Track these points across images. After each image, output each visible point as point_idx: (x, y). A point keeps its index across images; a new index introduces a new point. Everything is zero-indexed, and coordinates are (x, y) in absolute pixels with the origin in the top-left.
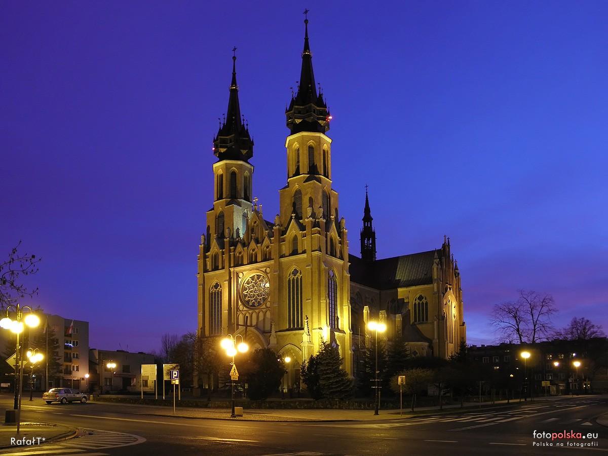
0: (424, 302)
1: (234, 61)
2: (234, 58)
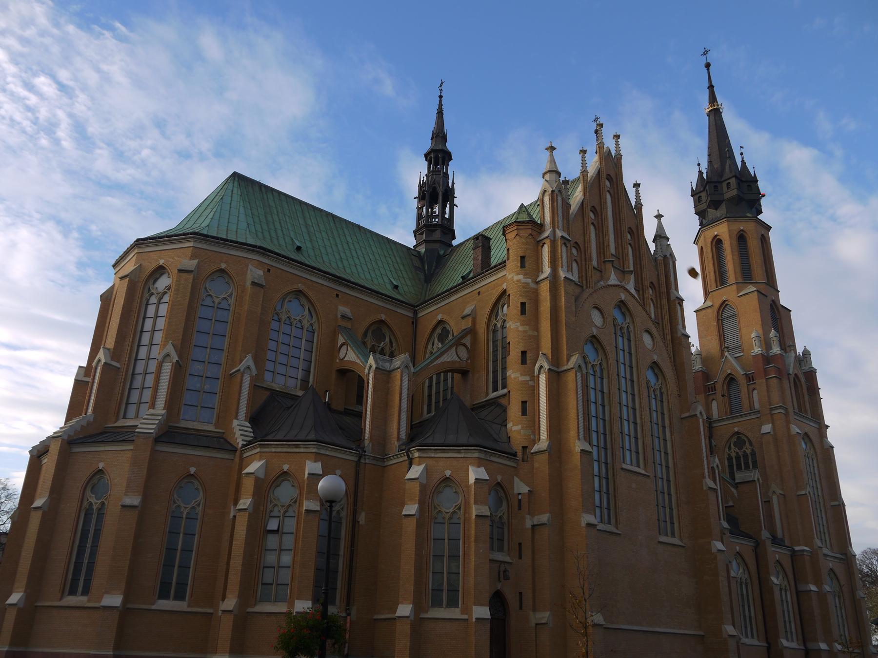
0: (749, 451)
1: (708, 70)
2: (708, 66)
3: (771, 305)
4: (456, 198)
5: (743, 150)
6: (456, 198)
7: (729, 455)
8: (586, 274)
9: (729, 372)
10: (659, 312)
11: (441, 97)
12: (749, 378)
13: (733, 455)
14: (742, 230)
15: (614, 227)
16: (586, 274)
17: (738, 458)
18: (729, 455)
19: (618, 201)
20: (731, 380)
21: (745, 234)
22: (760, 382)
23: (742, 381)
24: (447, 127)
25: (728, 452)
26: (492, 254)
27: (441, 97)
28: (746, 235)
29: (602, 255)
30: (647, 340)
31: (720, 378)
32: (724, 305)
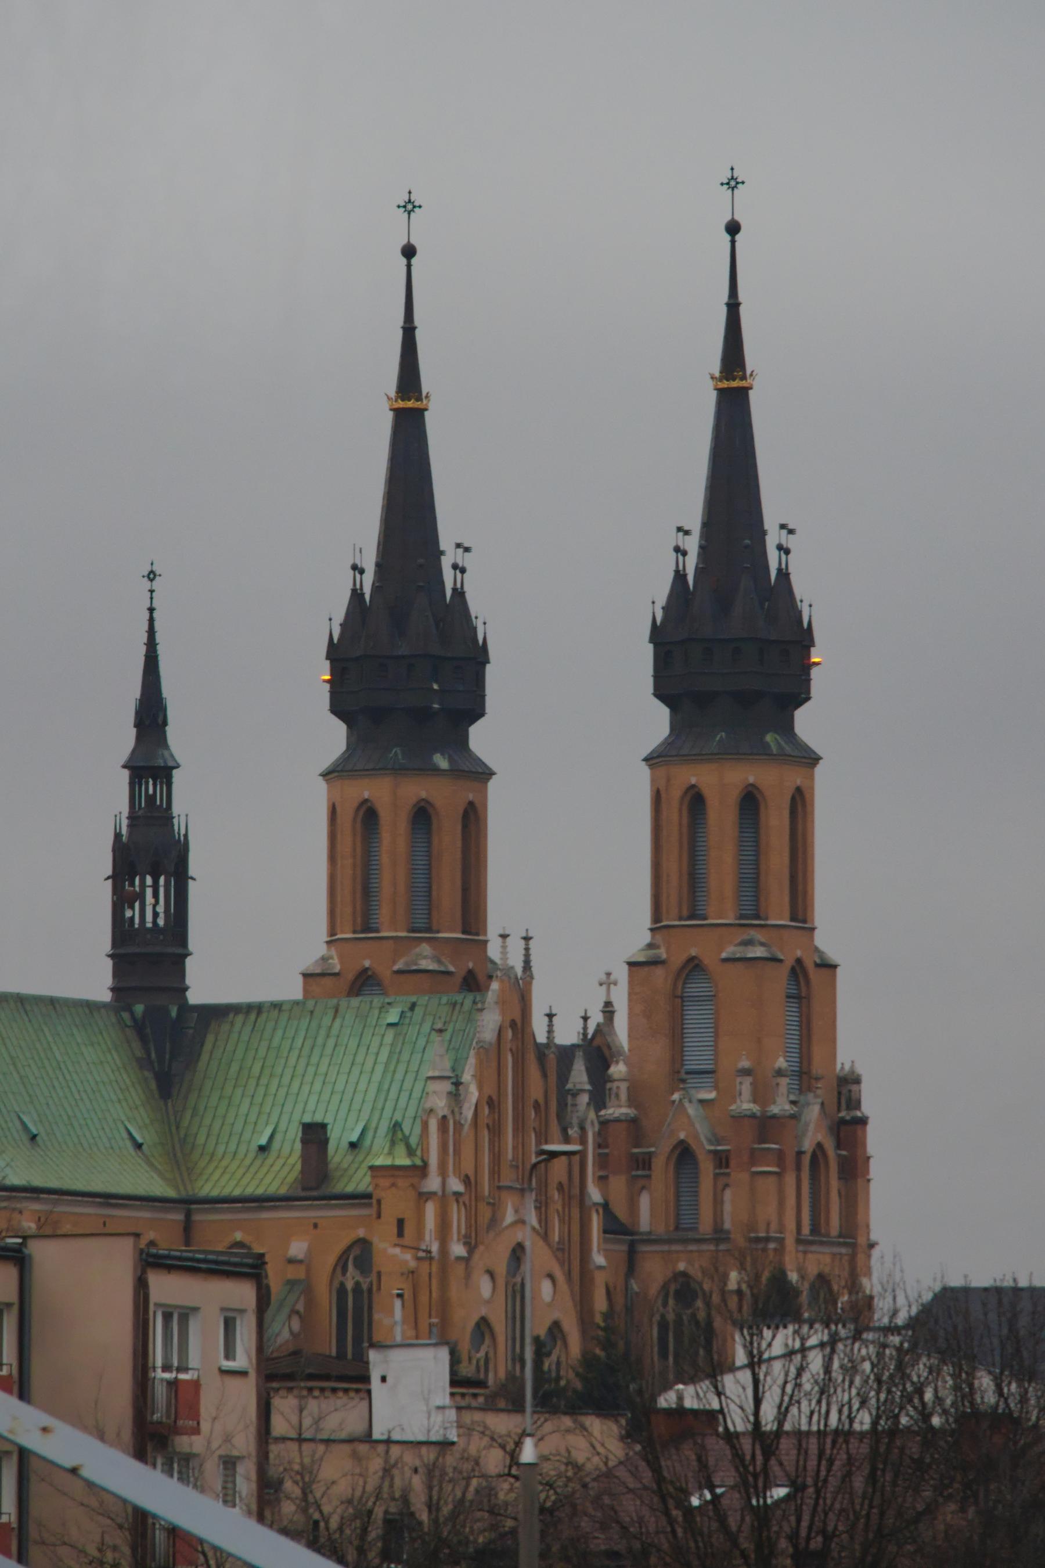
3: (793, 799)
4: (193, 879)
5: (791, 542)
6: (193, 879)
7: (663, 1316)
8: (476, 1222)
9: (682, 1136)
10: (566, 1230)
11: (151, 610)
12: (721, 1159)
13: (349, 1285)
14: (752, 785)
15: (483, 763)
16: (476, 1222)
17: (679, 1321)
18: (663, 1316)
19: (546, 1186)
20: (684, 1154)
21: (755, 792)
22: (739, 1176)
23: (707, 1168)
24: (168, 689)
25: (661, 1308)
26: (298, 1167)
27: (151, 610)
28: (758, 796)
29: (496, 1176)
30: (546, 1288)
31: (662, 1151)
32: (693, 967)
